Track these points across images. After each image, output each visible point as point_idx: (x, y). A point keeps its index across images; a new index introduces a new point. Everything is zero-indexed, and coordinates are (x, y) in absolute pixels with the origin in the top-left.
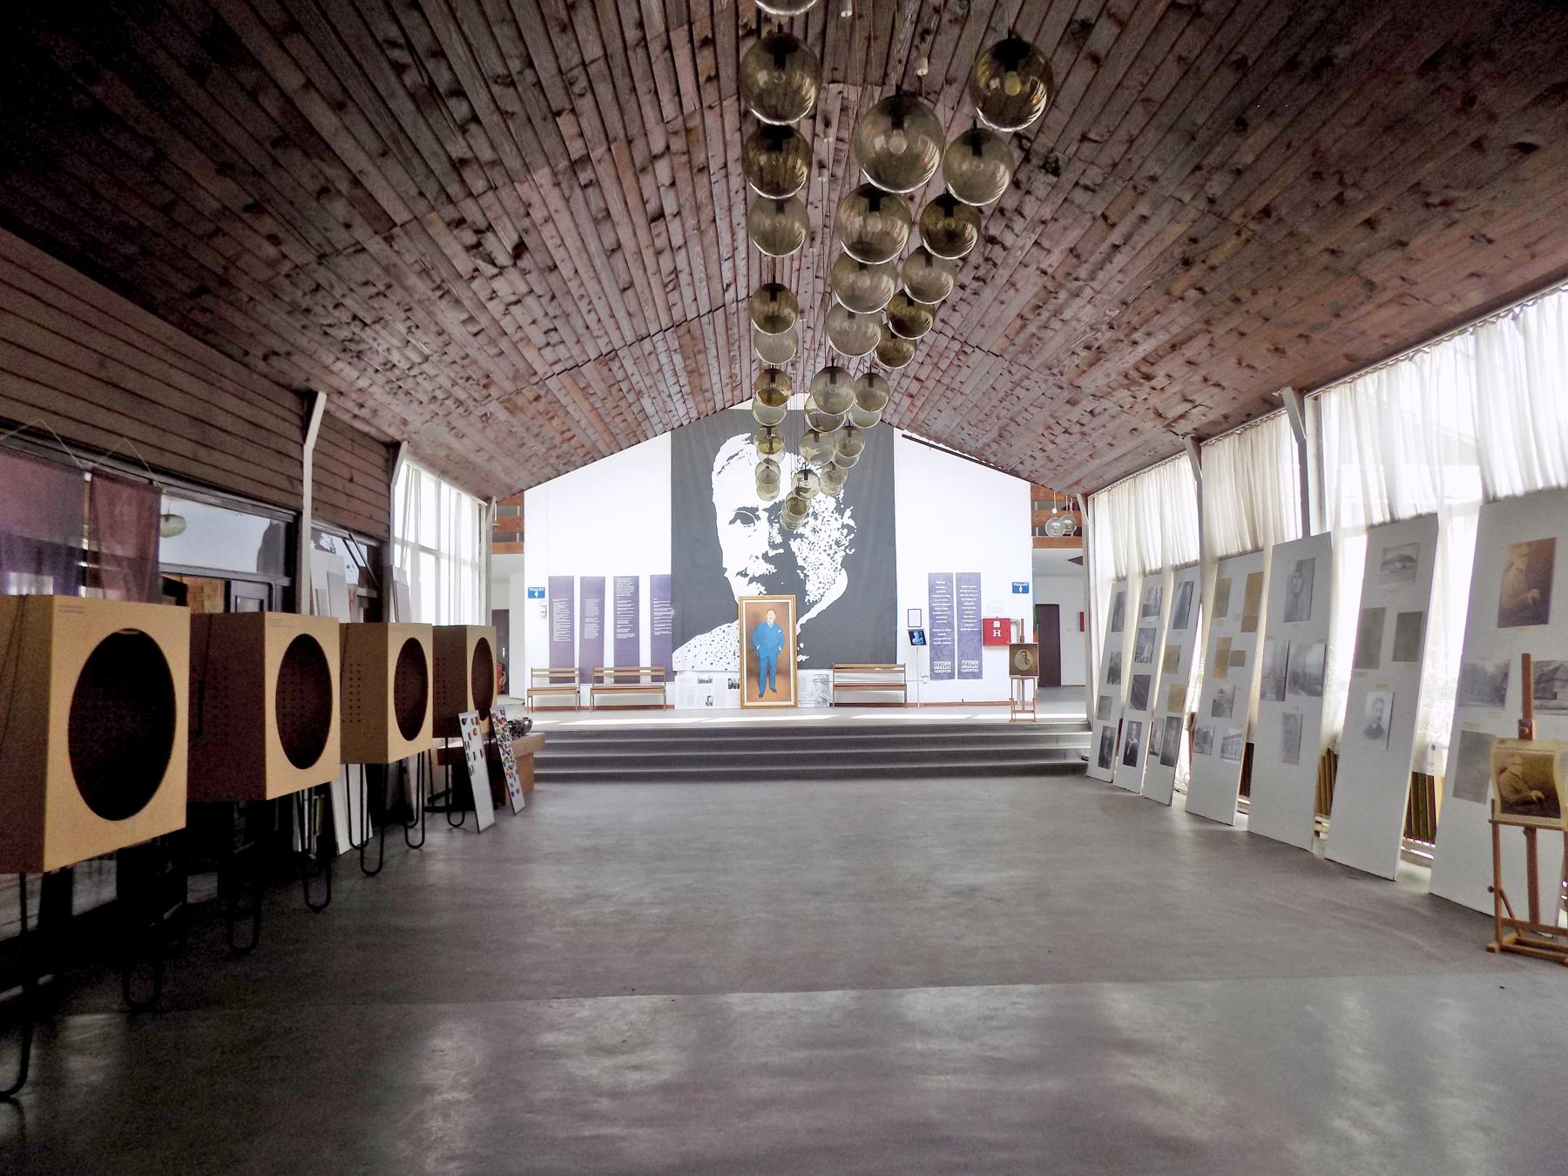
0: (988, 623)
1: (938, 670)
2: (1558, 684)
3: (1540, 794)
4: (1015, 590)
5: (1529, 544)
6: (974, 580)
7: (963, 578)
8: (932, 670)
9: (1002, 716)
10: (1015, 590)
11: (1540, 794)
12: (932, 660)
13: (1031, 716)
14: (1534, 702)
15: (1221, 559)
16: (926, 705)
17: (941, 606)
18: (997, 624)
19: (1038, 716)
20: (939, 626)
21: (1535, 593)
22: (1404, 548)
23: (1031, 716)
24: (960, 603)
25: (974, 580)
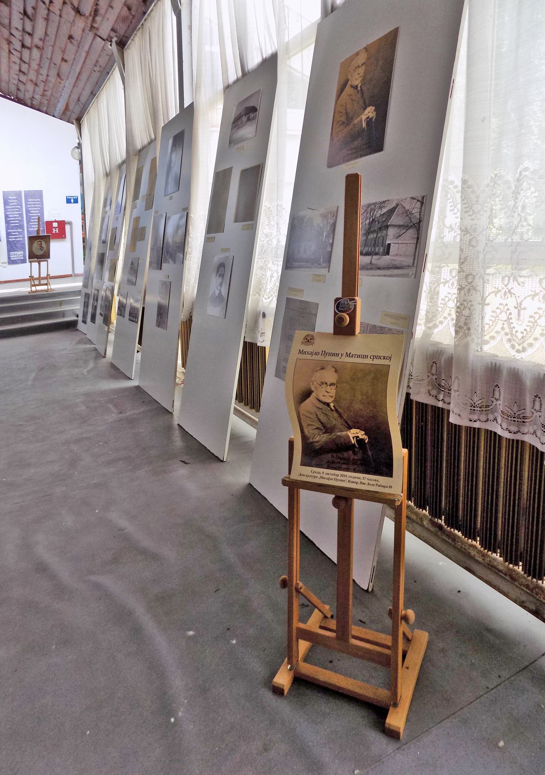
0: (49, 224)
1: (13, 257)
2: (391, 232)
3: (361, 434)
4: (68, 201)
5: (366, 49)
6: (38, 195)
7: (30, 195)
8: (9, 258)
9: (25, 289)
10: (68, 201)
11: (361, 434)
12: (9, 251)
13: (45, 287)
14: (363, 260)
15: (140, 151)
16: (5, 282)
17: (13, 214)
18: (55, 225)
19: (53, 286)
20: (13, 228)
21: (370, 112)
22: (250, 104)
23: (45, 287)
24: (28, 212)
25: (38, 195)
